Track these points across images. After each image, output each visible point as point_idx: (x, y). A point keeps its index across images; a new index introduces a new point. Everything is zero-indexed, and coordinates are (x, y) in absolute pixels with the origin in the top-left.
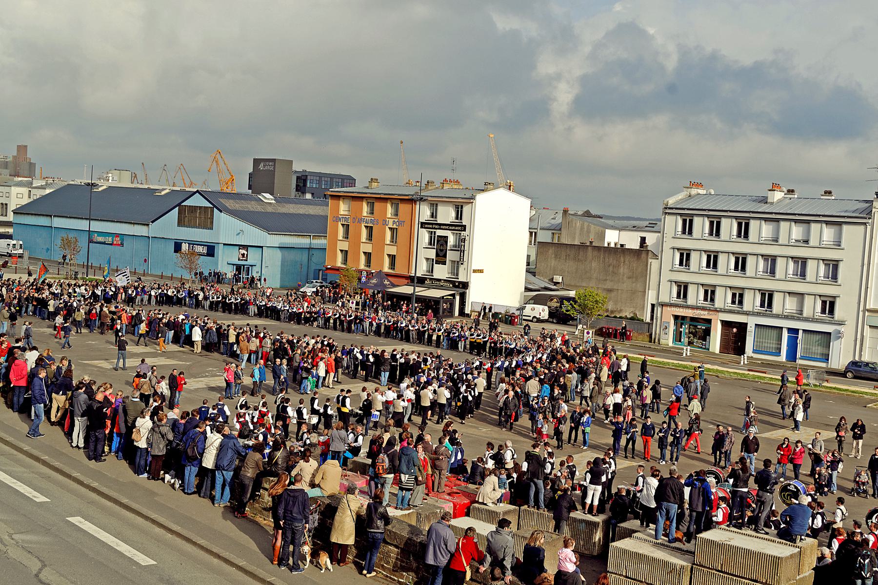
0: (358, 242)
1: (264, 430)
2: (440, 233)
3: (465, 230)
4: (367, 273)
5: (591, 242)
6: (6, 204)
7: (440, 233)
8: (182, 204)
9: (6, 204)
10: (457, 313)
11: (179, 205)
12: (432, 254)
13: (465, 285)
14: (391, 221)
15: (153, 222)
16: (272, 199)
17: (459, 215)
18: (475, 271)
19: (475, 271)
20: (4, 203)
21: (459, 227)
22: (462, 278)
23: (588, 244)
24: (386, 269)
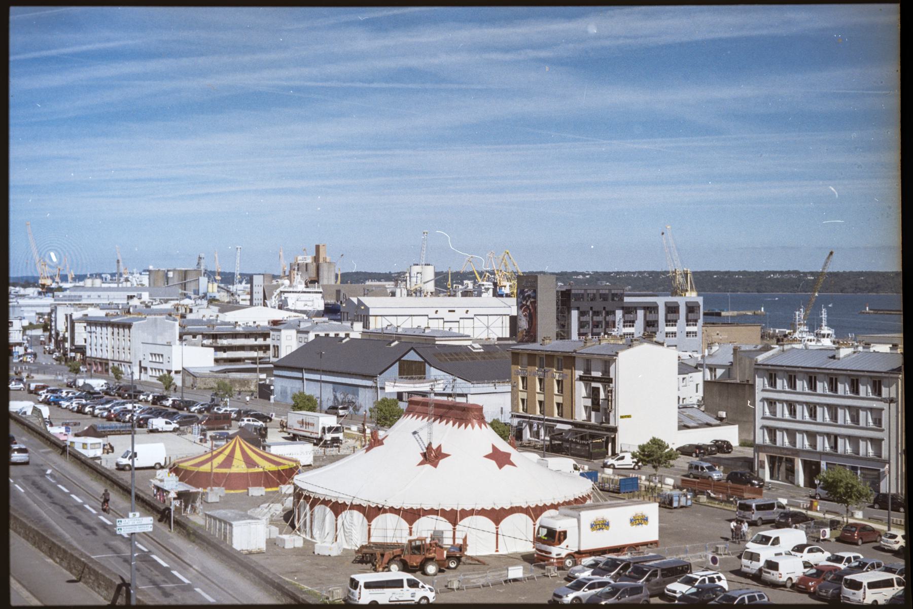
0: (534, 393)
1: (832, 575)
2: (594, 385)
3: (612, 383)
4: (295, 489)
5: (748, 381)
6: (278, 347)
7: (594, 385)
8: (402, 359)
9: (278, 347)
10: (610, 453)
11: (399, 360)
12: (589, 402)
13: (615, 430)
14: (557, 375)
15: (380, 374)
16: (480, 349)
17: (606, 372)
18: (622, 417)
19: (622, 417)
20: (276, 345)
21: (607, 380)
22: (612, 424)
23: (745, 383)
24: (556, 416)
